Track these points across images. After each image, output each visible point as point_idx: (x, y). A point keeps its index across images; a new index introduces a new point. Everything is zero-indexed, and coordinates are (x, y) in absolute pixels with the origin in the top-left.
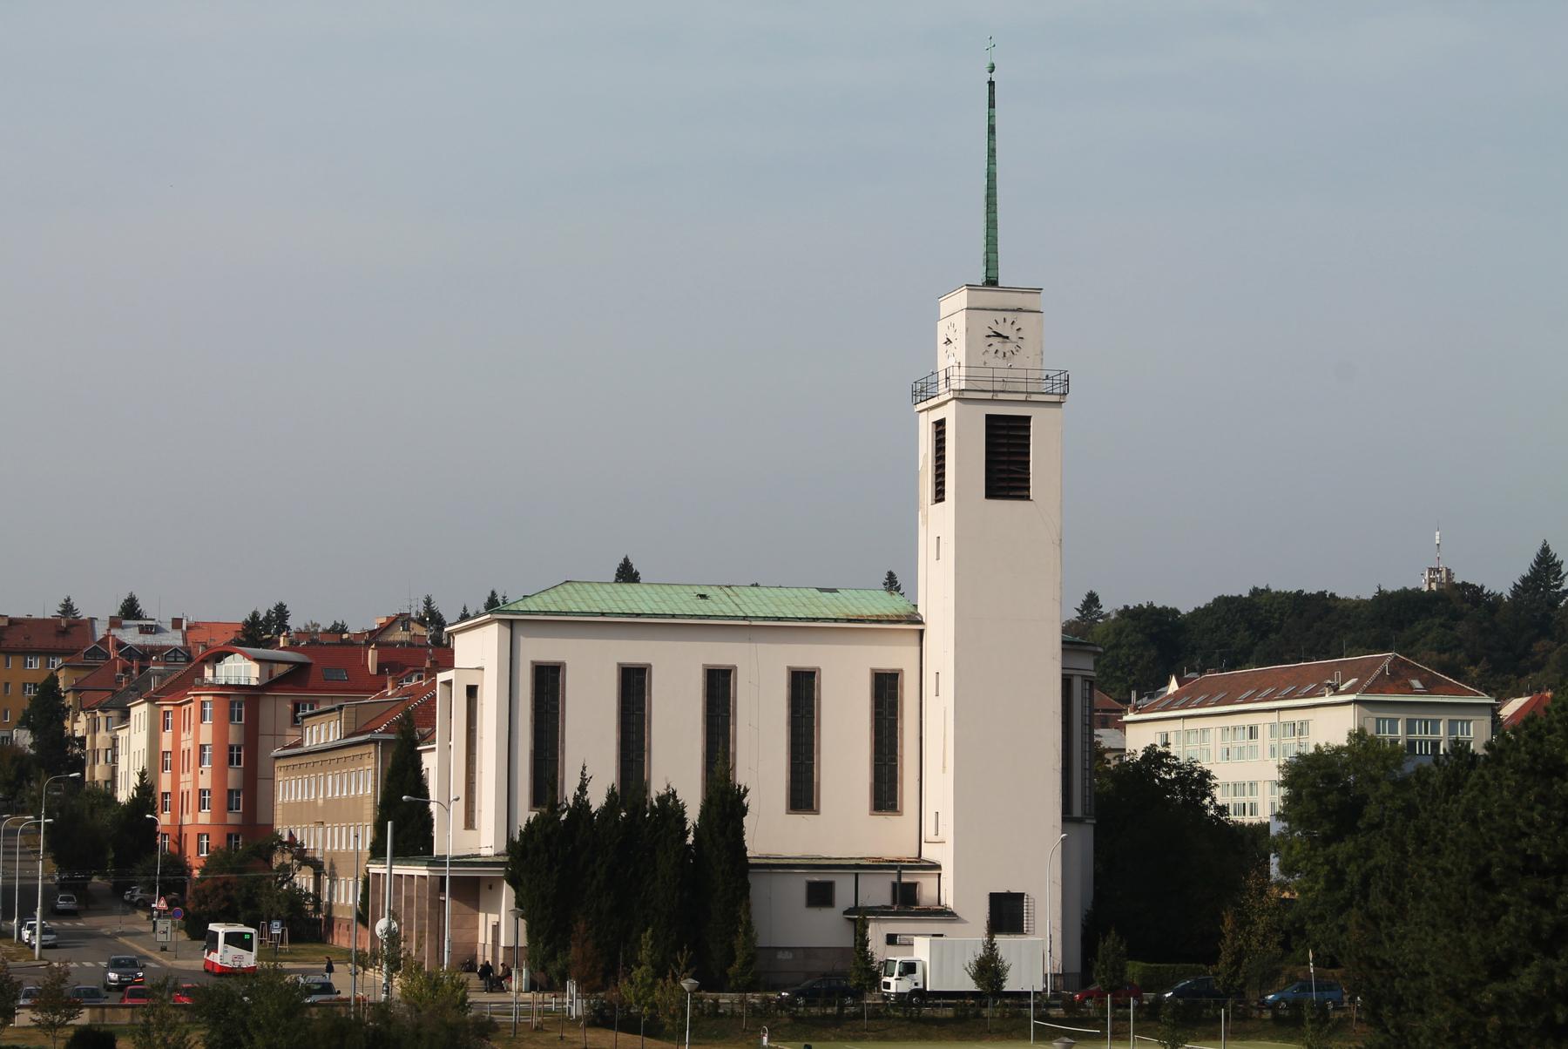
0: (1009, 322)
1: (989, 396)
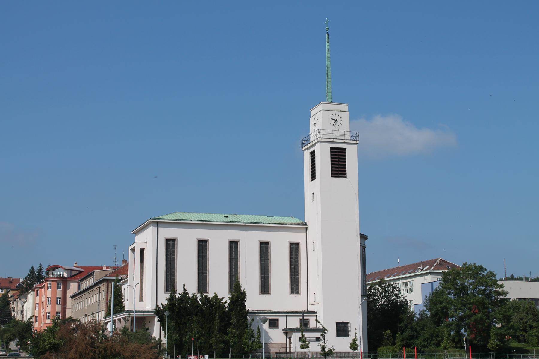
0: (337, 115)
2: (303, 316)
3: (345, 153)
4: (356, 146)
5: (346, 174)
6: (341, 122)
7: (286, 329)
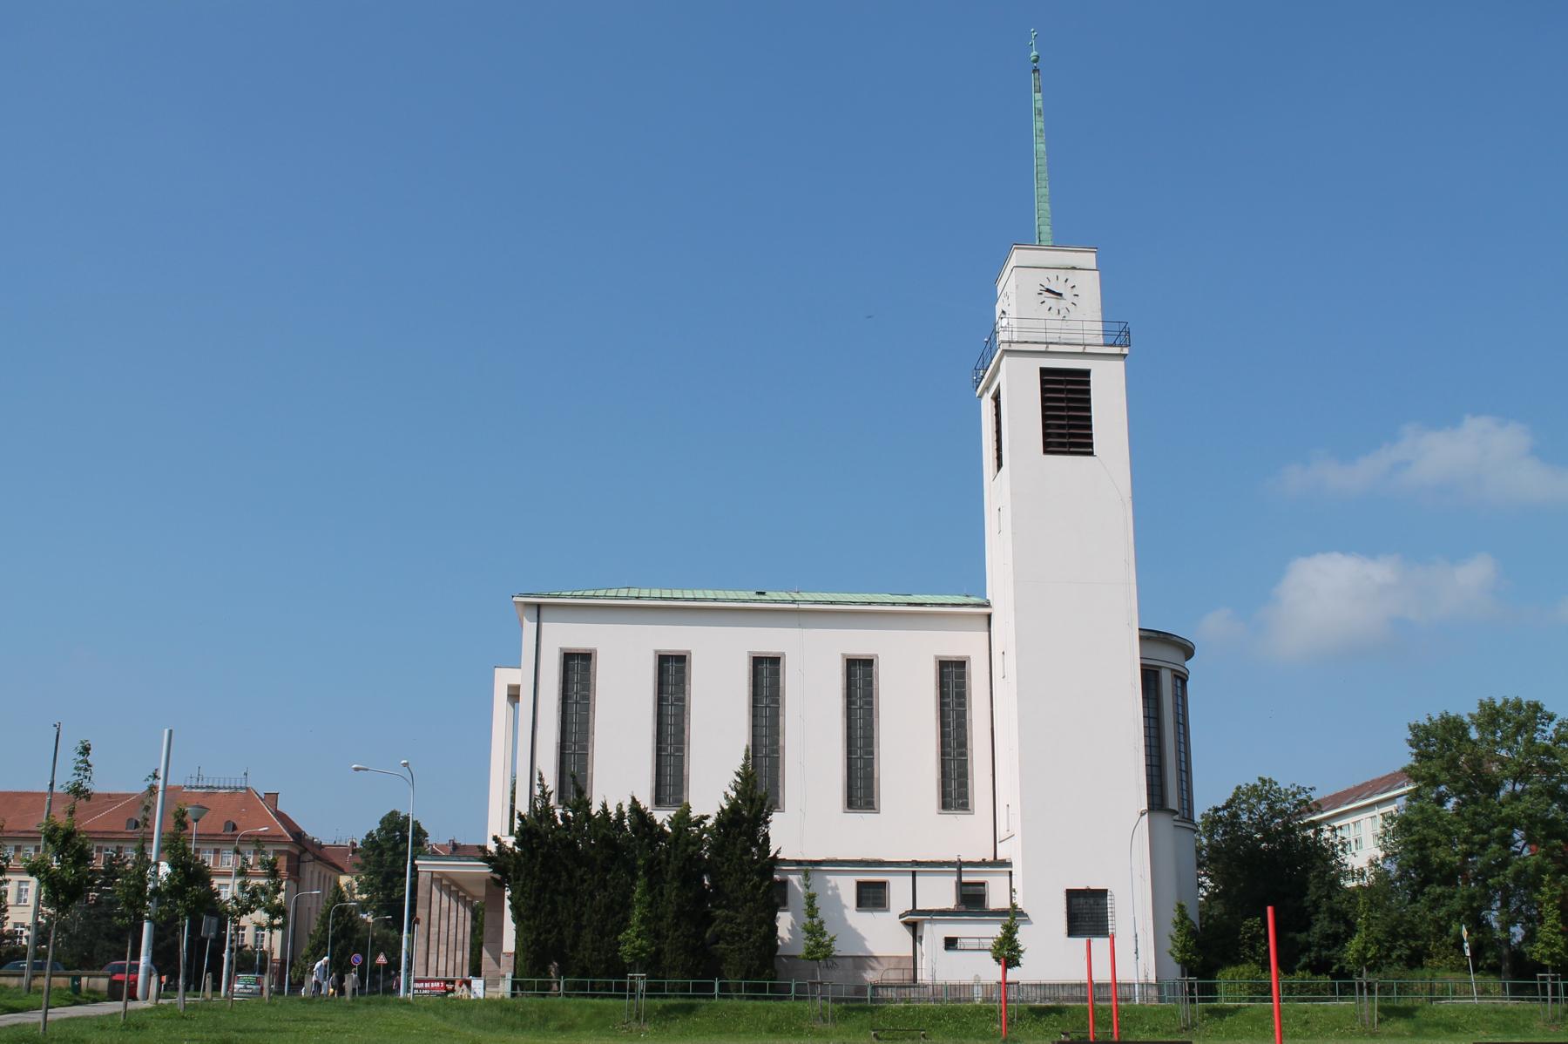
1: (1042, 348)
2: (960, 874)
3: (1088, 383)
4: (1120, 364)
5: (1091, 445)
6: (1075, 300)
7: (914, 911)
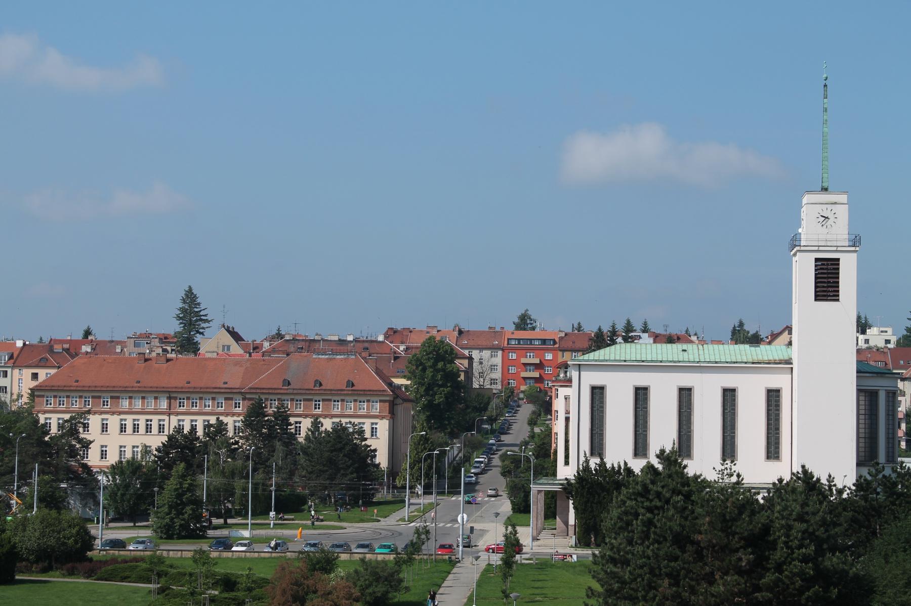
0: (829, 210)
1: (816, 248)
4: (855, 255)
